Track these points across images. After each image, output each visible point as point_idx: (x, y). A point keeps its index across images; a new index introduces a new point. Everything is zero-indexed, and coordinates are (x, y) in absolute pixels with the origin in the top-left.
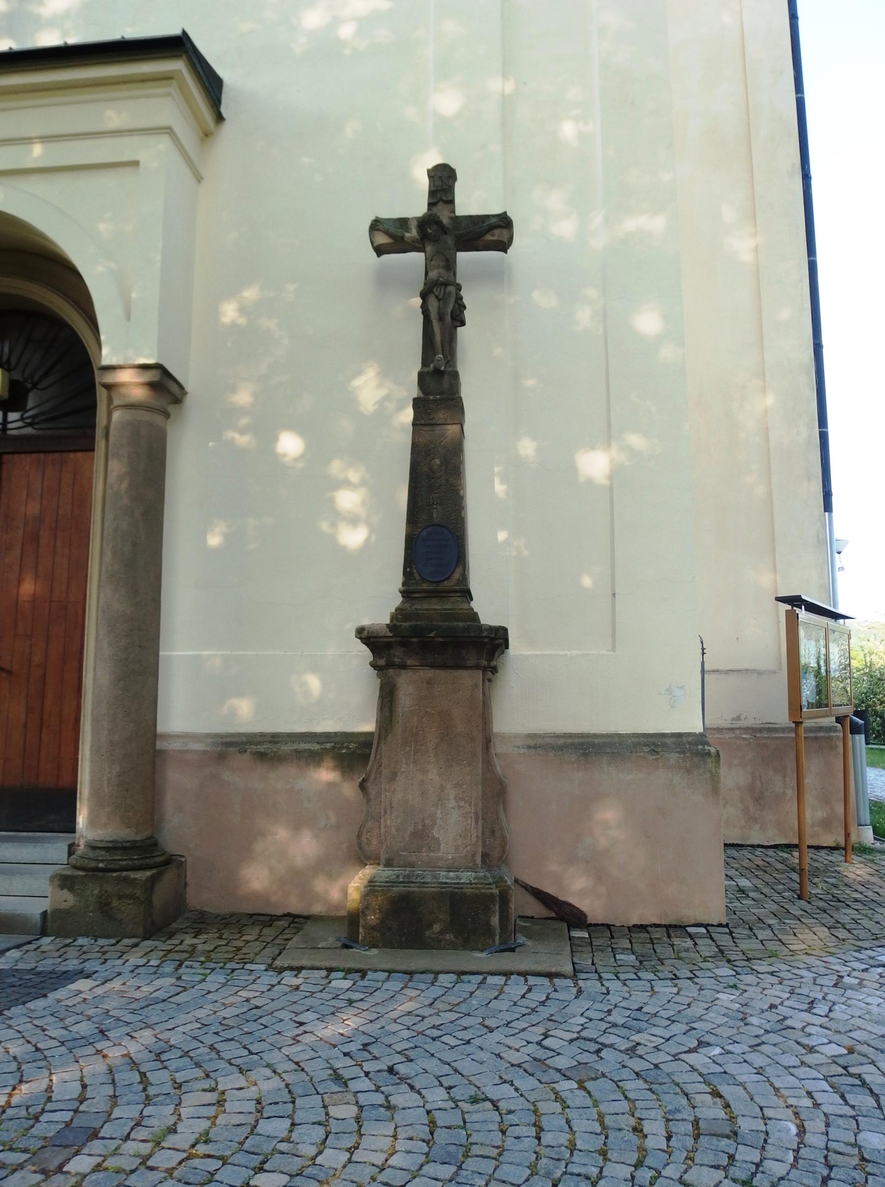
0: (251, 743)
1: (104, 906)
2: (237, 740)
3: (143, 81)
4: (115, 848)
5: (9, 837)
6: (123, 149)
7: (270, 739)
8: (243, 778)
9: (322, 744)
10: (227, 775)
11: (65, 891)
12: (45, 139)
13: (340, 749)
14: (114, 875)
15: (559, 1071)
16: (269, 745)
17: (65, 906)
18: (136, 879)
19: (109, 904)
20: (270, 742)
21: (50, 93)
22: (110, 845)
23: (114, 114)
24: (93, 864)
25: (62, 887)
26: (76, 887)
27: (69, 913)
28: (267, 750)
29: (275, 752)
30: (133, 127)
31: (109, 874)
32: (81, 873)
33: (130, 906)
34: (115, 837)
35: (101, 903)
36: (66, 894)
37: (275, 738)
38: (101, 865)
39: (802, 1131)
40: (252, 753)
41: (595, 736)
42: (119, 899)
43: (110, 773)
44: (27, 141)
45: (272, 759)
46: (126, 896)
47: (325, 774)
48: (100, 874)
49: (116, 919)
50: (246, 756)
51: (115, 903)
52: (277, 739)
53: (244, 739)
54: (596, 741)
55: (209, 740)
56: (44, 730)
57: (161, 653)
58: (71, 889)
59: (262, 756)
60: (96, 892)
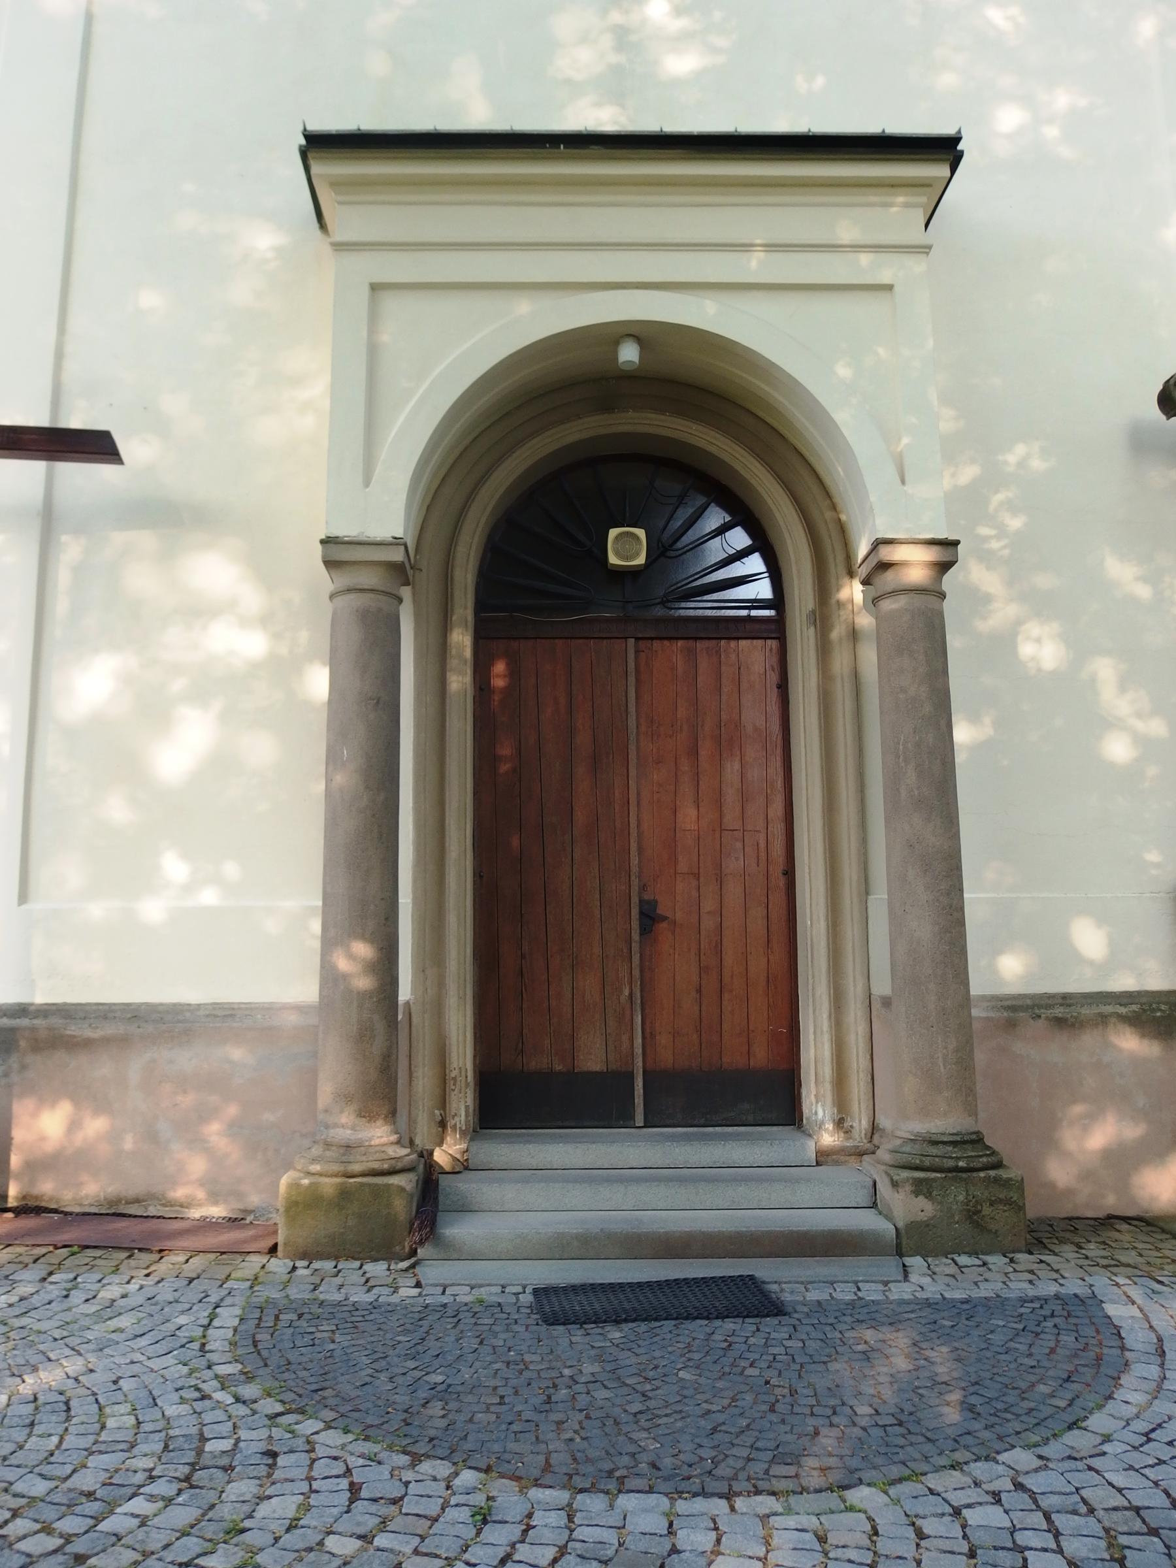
0: (1040, 1007)
1: (973, 1215)
2: (1020, 1003)
3: (831, 185)
4: (964, 1142)
5: (685, 1134)
6: (866, 267)
7: (1060, 1001)
8: (1038, 1050)
9: (1125, 1005)
10: (1019, 1047)
11: (921, 1198)
12: (771, 247)
13: (1154, 1010)
14: (982, 1174)
15: (606, 1387)
16: (1061, 1009)
17: (923, 1217)
18: (1010, 1179)
19: (980, 1211)
20: (1061, 1005)
21: (863, 189)
22: (958, 1138)
23: (847, 223)
24: (951, 1163)
25: (917, 1193)
26: (935, 1193)
27: (928, 1226)
28: (1063, 1014)
29: (1076, 1018)
30: (862, 243)
31: (975, 1174)
32: (939, 1175)
33: (1007, 1214)
34: (958, 1129)
35: (969, 1211)
36: (922, 1202)
37: (1066, 999)
38: (961, 1164)
39: (923, 1435)
40: (1047, 1018)
41: (114, 1004)
42: (991, 1205)
43: (946, 1048)
44: (746, 247)
45: (1073, 1025)
46: (1000, 1201)
47: (1130, 1043)
48: (964, 1175)
49: (990, 1231)
50: (1040, 1022)
51: (987, 1210)
52: (1068, 1001)
53: (1029, 1002)
54: (88, 1008)
55: (985, 1004)
56: (726, 996)
57: (320, 903)
58: (929, 1196)
59: (1060, 1023)
60: (961, 1198)
